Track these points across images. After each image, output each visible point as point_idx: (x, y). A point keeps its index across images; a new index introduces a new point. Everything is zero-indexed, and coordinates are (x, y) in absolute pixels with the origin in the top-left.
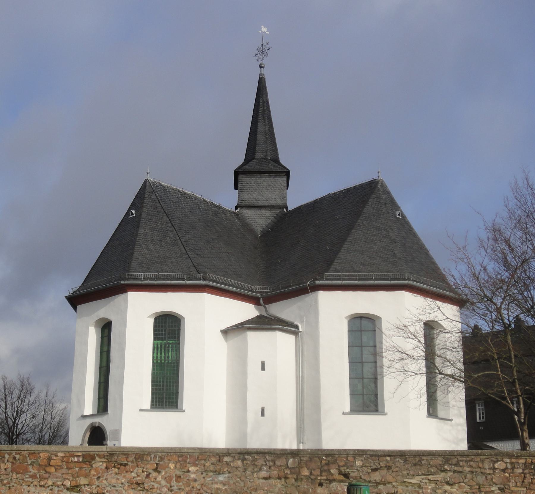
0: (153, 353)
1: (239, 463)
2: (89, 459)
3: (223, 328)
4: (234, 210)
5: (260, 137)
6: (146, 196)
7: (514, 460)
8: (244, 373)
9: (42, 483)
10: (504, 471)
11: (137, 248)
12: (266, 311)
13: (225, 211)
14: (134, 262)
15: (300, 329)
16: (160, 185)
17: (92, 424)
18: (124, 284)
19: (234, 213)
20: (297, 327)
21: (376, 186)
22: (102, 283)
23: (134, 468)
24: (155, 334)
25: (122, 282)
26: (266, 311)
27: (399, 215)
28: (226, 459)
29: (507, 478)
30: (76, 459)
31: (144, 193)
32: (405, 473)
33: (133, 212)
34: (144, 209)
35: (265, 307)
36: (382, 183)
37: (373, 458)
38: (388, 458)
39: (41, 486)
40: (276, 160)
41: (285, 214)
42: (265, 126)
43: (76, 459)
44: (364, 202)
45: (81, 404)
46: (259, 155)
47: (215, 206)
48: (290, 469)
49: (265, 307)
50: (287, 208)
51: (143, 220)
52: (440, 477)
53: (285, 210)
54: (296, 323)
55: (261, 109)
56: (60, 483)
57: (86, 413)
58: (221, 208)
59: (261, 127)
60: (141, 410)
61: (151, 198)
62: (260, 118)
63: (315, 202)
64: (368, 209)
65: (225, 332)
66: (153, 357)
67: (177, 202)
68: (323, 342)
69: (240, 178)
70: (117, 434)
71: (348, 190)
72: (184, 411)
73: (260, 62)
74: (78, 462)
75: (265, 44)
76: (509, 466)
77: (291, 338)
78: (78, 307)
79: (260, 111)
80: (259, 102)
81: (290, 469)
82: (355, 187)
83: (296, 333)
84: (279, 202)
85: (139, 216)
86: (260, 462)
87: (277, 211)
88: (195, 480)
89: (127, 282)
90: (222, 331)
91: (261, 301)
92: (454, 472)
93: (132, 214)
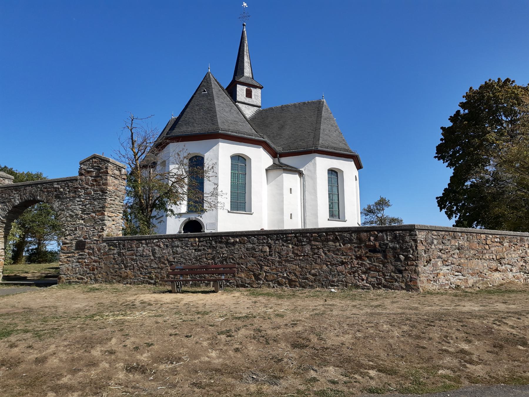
70: (215, 224)
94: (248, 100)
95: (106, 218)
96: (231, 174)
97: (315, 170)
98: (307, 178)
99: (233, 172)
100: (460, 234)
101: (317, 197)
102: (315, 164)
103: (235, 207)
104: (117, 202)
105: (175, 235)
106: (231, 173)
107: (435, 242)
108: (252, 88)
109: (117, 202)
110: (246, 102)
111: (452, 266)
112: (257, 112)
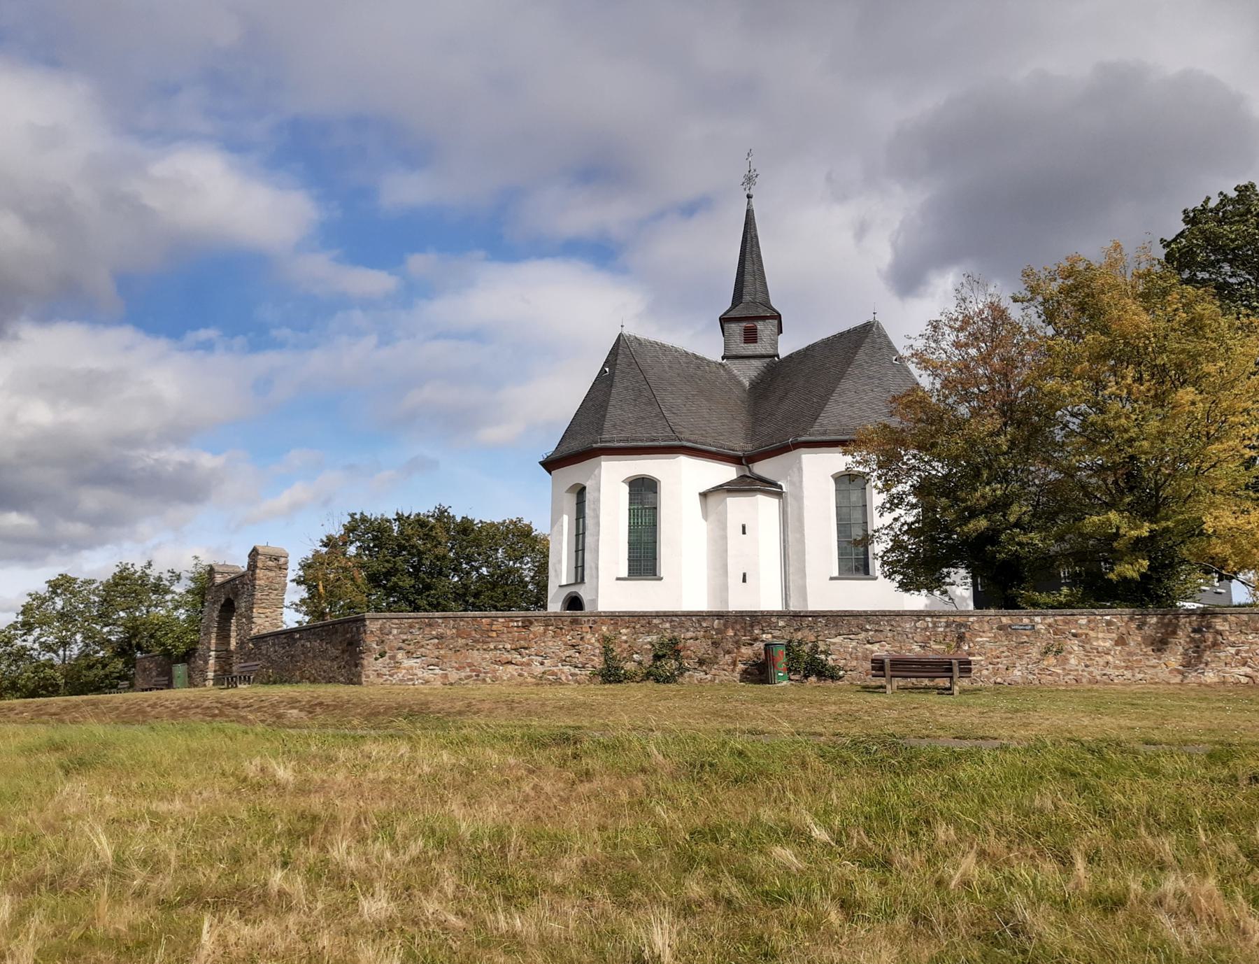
0: (630, 519)
1: (668, 625)
2: (527, 623)
3: (703, 490)
4: (720, 360)
5: (748, 278)
6: (620, 351)
7: (935, 619)
8: (725, 538)
9: (485, 647)
10: (926, 629)
11: (610, 409)
12: (750, 471)
13: (709, 363)
14: (607, 425)
15: (784, 490)
16: (636, 338)
17: (569, 594)
18: (596, 448)
19: (720, 364)
20: (781, 487)
21: (871, 330)
22: (575, 446)
23: (569, 631)
24: (630, 499)
25: (594, 445)
26: (750, 471)
27: (896, 360)
28: (656, 621)
29: (928, 636)
30: (515, 624)
31: (618, 349)
32: (826, 632)
33: (607, 369)
34: (618, 366)
35: (748, 467)
36: (878, 328)
37: (796, 618)
38: (810, 619)
39: (484, 650)
40: (767, 304)
41: (775, 363)
42: (754, 264)
43: (515, 624)
44: (858, 346)
45: (558, 575)
46: (747, 298)
47: (697, 358)
48: (715, 630)
49: (748, 467)
50: (778, 356)
51: (616, 379)
52: (862, 635)
53: (776, 359)
54: (779, 483)
55: (748, 246)
56: (501, 647)
57: (564, 582)
58: (706, 359)
59: (748, 266)
60: (618, 579)
61: (624, 354)
62: (748, 256)
63: (807, 349)
64: (861, 356)
65: (704, 495)
66: (630, 523)
67: (655, 356)
68: (806, 502)
69: (726, 326)
70: (595, 601)
71: (842, 334)
72: (661, 579)
73: (747, 192)
74: (518, 627)
75: (752, 171)
76: (930, 625)
77: (773, 503)
78: (553, 472)
79: (748, 250)
80: (746, 238)
81: (715, 630)
82: (849, 331)
83: (779, 494)
84: (771, 352)
85: (612, 374)
86: (688, 624)
87: (768, 360)
88: (626, 642)
89: (599, 445)
90: (700, 494)
91: (744, 462)
92: (876, 631)
93: (606, 372)
94: (751, 349)
95: (254, 615)
96: (630, 512)
97: (801, 482)
98: (790, 499)
99: (632, 507)
100: (440, 621)
101: (804, 535)
102: (800, 469)
103: (637, 570)
104: (272, 596)
105: (921, 611)
106: (630, 510)
107: (395, 632)
108: (755, 323)
109: (272, 596)
110: (750, 353)
111: (423, 658)
112: (769, 368)
